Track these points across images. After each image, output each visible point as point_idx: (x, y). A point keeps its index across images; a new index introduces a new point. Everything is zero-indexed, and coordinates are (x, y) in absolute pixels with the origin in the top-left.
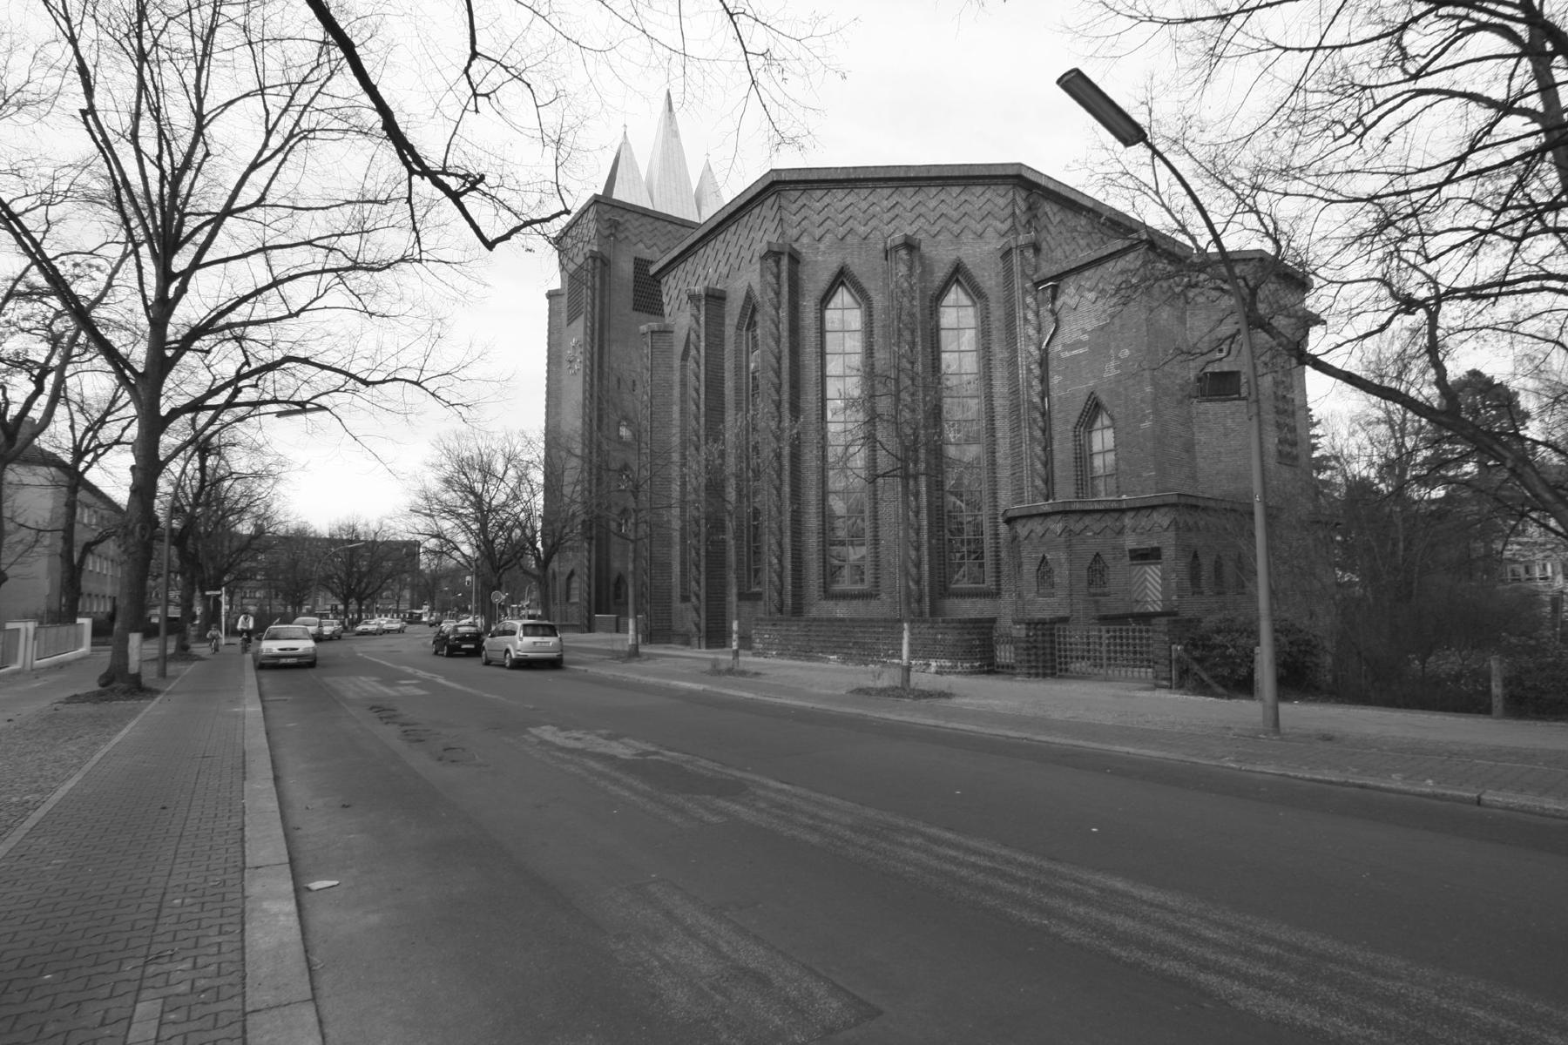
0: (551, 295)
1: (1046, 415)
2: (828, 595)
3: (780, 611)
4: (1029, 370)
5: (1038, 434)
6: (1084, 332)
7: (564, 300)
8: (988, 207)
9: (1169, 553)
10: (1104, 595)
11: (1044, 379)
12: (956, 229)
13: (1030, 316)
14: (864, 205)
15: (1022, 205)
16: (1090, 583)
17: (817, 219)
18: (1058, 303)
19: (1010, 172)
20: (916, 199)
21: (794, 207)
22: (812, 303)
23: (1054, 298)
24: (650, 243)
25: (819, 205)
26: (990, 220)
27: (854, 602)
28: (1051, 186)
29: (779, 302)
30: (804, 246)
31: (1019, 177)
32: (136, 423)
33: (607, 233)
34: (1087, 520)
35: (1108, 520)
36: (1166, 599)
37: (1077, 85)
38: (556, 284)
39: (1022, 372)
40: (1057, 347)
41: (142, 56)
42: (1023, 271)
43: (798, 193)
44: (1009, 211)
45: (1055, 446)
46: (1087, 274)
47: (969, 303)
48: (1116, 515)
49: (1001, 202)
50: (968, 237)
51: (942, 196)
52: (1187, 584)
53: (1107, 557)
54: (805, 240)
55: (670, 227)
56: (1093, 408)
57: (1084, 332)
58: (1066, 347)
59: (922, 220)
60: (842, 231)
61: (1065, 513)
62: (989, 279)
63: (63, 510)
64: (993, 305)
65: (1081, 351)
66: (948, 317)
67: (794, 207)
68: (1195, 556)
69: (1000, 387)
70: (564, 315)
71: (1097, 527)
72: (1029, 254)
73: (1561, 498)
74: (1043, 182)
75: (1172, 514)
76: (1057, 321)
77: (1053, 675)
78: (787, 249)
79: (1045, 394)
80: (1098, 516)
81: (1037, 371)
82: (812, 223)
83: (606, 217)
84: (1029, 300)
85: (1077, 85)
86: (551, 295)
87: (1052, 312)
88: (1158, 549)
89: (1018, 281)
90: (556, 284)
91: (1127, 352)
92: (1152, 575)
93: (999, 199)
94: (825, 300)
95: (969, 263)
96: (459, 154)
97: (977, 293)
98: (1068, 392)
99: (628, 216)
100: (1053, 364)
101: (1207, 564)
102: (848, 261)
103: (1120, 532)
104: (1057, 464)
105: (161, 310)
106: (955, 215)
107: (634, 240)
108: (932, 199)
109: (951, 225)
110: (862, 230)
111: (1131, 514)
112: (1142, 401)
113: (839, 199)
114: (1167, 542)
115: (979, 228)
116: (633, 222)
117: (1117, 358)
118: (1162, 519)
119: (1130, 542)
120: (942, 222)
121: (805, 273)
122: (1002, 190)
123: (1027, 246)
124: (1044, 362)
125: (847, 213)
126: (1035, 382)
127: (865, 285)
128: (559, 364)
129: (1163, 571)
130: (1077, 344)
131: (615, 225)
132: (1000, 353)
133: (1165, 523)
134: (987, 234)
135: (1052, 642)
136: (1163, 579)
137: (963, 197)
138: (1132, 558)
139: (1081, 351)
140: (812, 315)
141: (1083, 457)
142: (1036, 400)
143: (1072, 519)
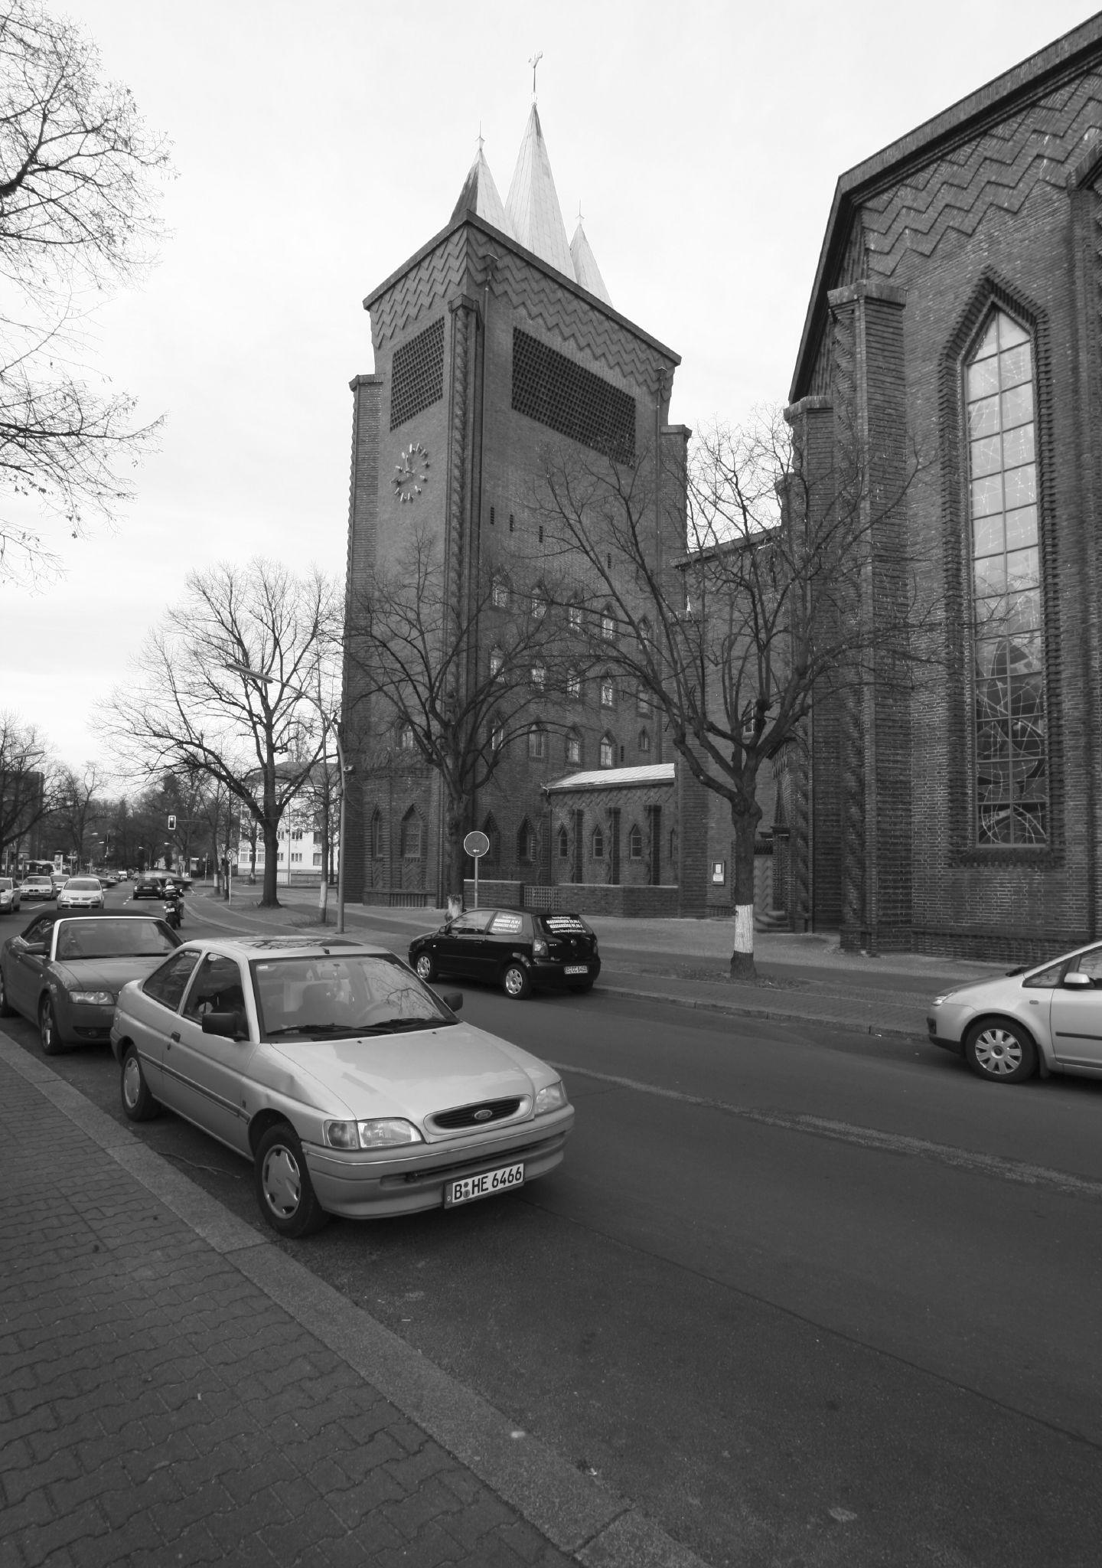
0: (359, 385)
7: (385, 392)
24: (535, 311)
32: (978, 357)
33: (480, 278)
37: (535, 107)
41: (923, 933)
55: (560, 294)
63: (1062, 250)
70: (384, 418)
73: (3, 435)
83: (481, 252)
85: (535, 107)
86: (359, 385)
90: (368, 368)
96: (980, 409)
99: (508, 260)
105: (264, 699)
107: (515, 300)
116: (517, 272)
128: (373, 488)
131: (490, 267)
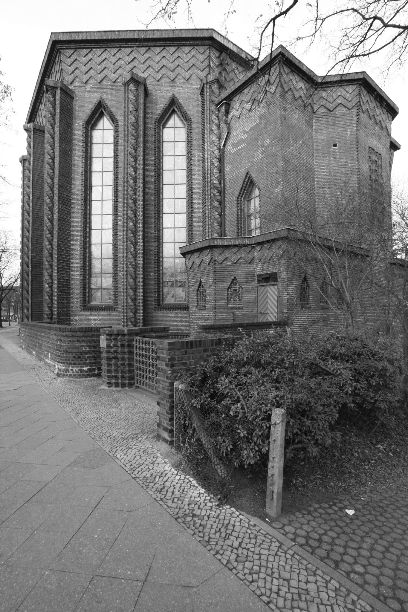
0: (23, 161)
1: (222, 192)
2: (87, 306)
3: (51, 318)
4: (212, 163)
5: (216, 204)
6: (244, 132)
8: (193, 61)
9: (282, 276)
10: (239, 308)
11: (221, 170)
12: (172, 75)
13: (214, 128)
14: (114, 59)
15: (215, 61)
16: (229, 300)
17: (85, 69)
18: (230, 116)
19: (206, 35)
20: (147, 56)
21: (70, 61)
22: (81, 124)
23: (227, 113)
25: (85, 60)
26: (194, 70)
27: (102, 313)
28: (236, 50)
29: (54, 120)
30: (76, 87)
31: (211, 39)
34: (227, 253)
35: (243, 254)
36: (280, 312)
38: (25, 153)
39: (208, 164)
40: (229, 147)
42: (210, 99)
43: (71, 51)
44: (206, 63)
45: (227, 212)
46: (246, 91)
47: (182, 125)
48: (248, 249)
49: (202, 57)
50: (180, 81)
51: (164, 53)
52: (296, 301)
53: (242, 281)
54: (77, 83)
56: (249, 185)
57: (244, 132)
58: (235, 145)
59: (151, 69)
60: (100, 77)
61: (211, 248)
62: (192, 108)
64: (194, 125)
65: (242, 146)
66: (168, 134)
67: (70, 61)
68: (305, 279)
69: (197, 177)
71: (234, 258)
72: (215, 87)
74: (229, 46)
75: (284, 245)
76: (229, 129)
77: (131, 385)
78: (59, 85)
79: (222, 178)
80: (235, 250)
81: (217, 163)
82: (81, 72)
84: (214, 118)
87: (226, 122)
88: (276, 274)
89: (207, 104)
91: (268, 141)
92: (271, 292)
93: (199, 56)
94: (91, 123)
95: (181, 98)
97: (186, 118)
98: (234, 175)
100: (227, 158)
101: (315, 285)
102: (104, 97)
103: (251, 262)
104: (227, 223)
106: (172, 66)
108: (156, 55)
109: (169, 73)
110: (113, 76)
111: (258, 248)
112: (277, 173)
113: (97, 55)
114: (281, 269)
115: (187, 75)
117: (263, 146)
118: (276, 250)
119: (258, 269)
120: (163, 71)
121: (77, 104)
122: (202, 49)
123: (212, 82)
124: (221, 160)
125: (104, 65)
126: (216, 171)
127: (114, 113)
129: (278, 290)
130: (242, 141)
132: (197, 155)
133: (281, 252)
134: (192, 79)
135: (131, 353)
136: (278, 297)
137: (177, 54)
138: (259, 281)
139: (242, 146)
140: (81, 132)
141: (243, 218)
142: (216, 181)
143: (216, 252)
